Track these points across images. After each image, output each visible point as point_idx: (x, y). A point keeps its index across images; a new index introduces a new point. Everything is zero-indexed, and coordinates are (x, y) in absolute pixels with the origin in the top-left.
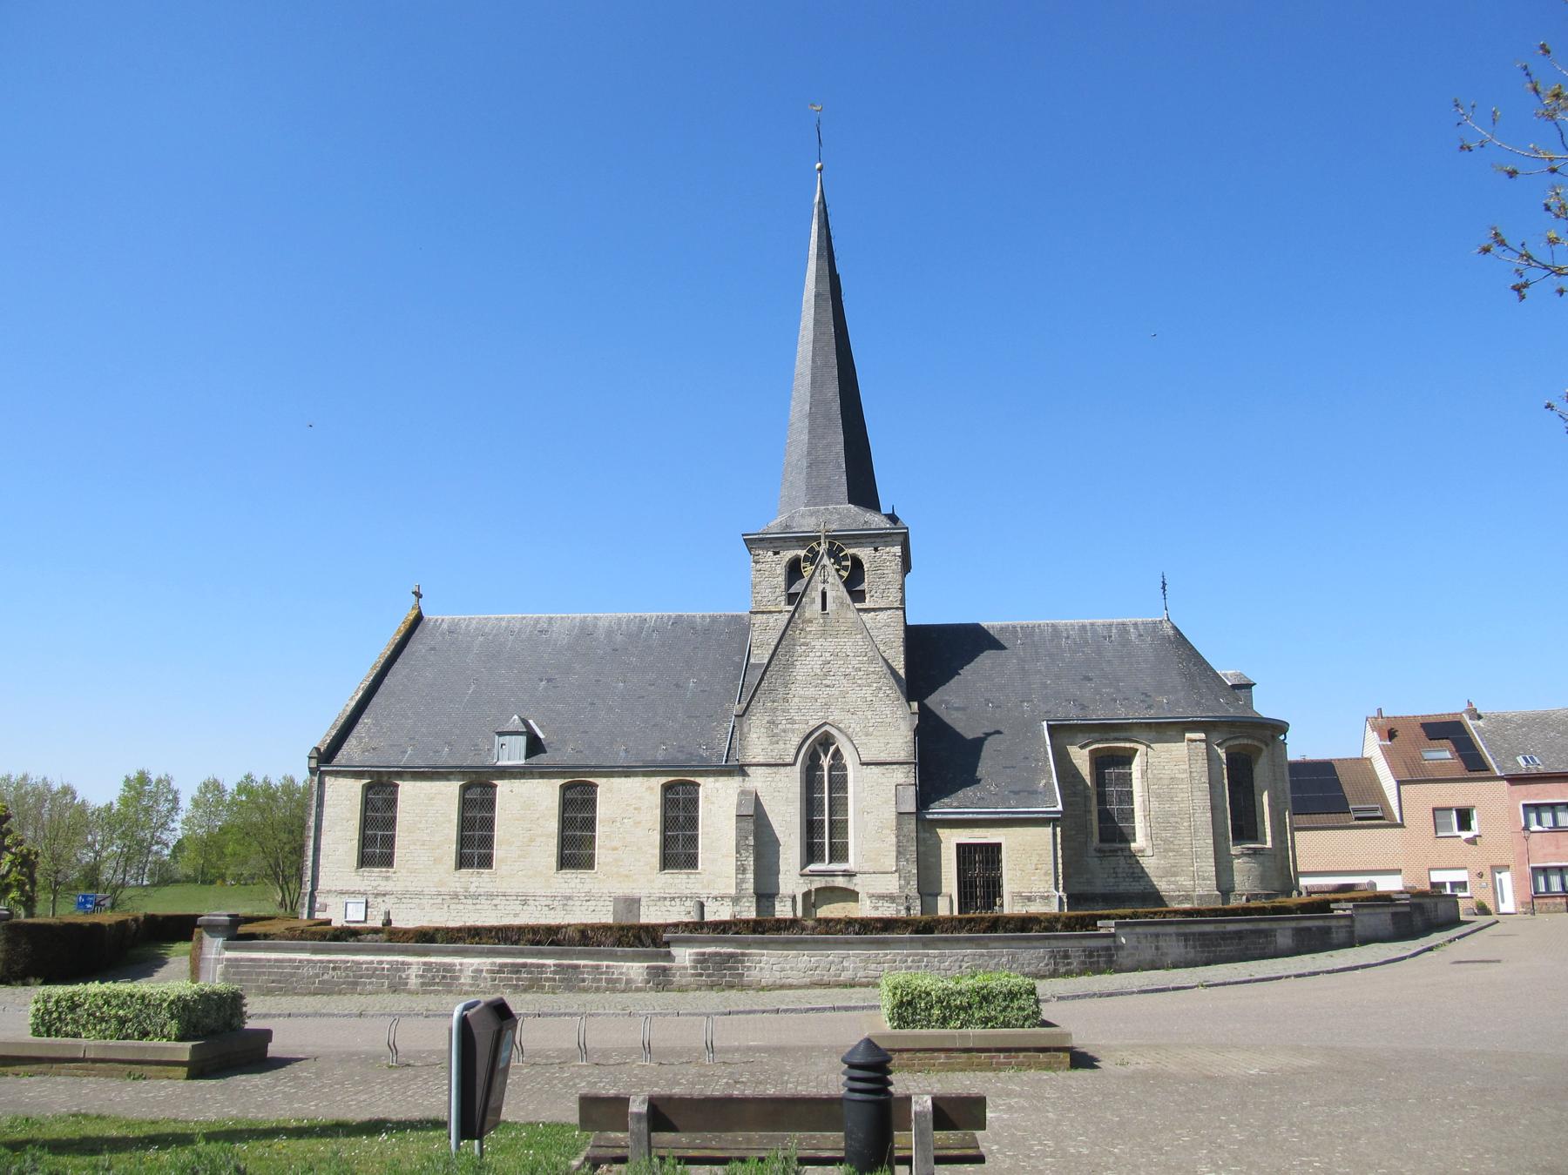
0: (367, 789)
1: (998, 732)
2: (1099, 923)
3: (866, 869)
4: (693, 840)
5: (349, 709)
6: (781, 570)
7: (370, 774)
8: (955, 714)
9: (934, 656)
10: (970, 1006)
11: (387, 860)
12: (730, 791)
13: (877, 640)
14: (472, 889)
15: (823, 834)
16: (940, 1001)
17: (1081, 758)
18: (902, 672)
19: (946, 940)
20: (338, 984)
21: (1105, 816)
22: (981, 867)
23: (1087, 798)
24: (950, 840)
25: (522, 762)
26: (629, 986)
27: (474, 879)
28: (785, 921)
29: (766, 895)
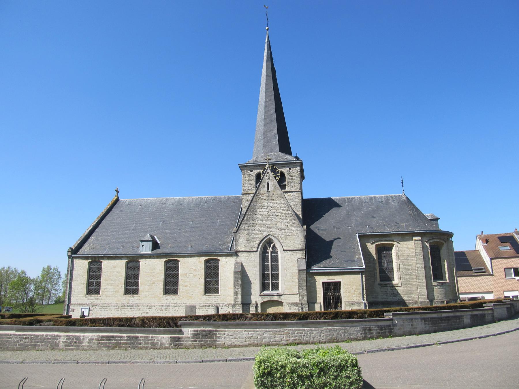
0: (90, 263)
1: (339, 238)
2: (385, 314)
4: (217, 282)
5: (86, 233)
6: (253, 178)
7: (91, 258)
8: (322, 232)
9: (313, 210)
10: (312, 375)
11: (97, 292)
13: (291, 204)
14: (130, 303)
15: (269, 279)
16: (293, 371)
17: (372, 248)
18: (301, 216)
19: (313, 323)
20: (27, 346)
21: (382, 271)
22: (333, 291)
23: (374, 264)
25: (150, 252)
26: (162, 347)
27: (131, 299)
28: (237, 315)
29: (246, 304)
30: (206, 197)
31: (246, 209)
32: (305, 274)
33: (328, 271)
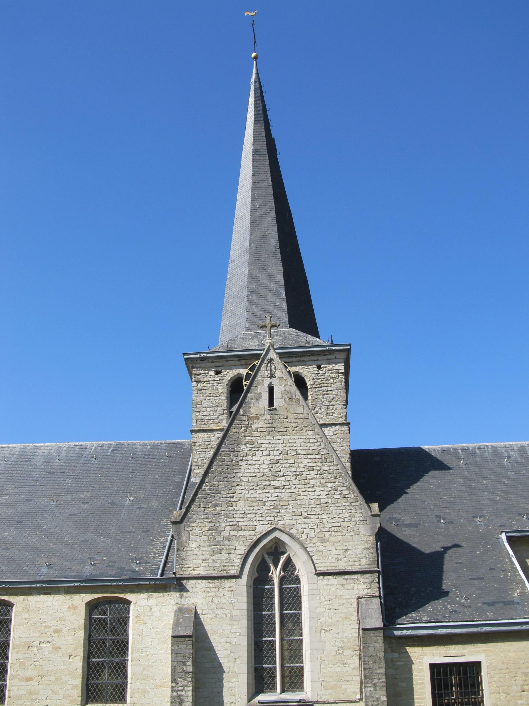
1: (457, 546)
3: (325, 698)
4: (121, 669)
6: (222, 389)
12: (166, 609)
24: (423, 660)
30: (95, 443)
31: (202, 471)
32: (381, 639)
33: (445, 631)
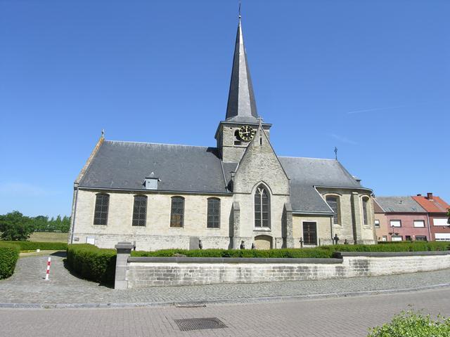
14: (137, 233)
